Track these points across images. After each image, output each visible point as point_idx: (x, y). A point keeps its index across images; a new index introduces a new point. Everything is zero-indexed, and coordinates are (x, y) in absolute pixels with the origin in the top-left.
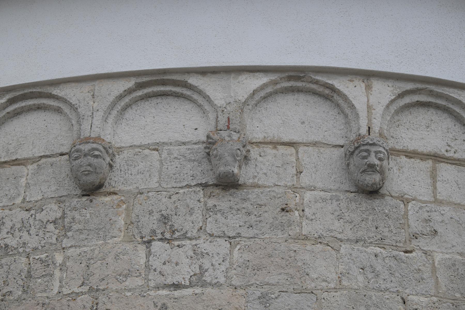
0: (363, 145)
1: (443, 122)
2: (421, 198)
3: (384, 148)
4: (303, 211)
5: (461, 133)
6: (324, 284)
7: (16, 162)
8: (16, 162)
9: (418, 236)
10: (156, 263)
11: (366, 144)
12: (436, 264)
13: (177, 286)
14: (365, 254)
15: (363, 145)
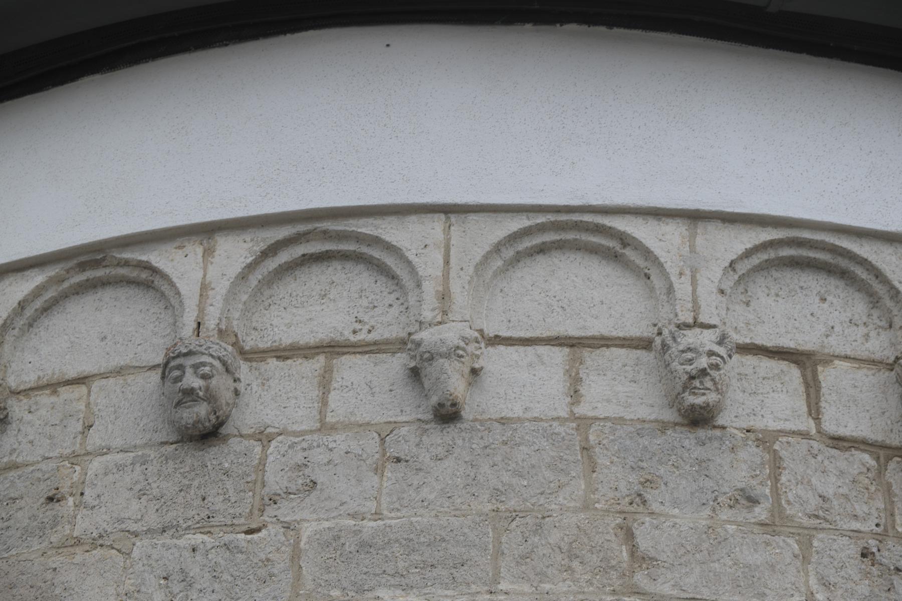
0: (174, 358)
1: (353, 281)
2: (296, 428)
3: (212, 356)
4: (82, 494)
5: (385, 294)
9: (277, 498)
11: (178, 356)
12: (302, 544)
14: (175, 550)
15: (174, 358)
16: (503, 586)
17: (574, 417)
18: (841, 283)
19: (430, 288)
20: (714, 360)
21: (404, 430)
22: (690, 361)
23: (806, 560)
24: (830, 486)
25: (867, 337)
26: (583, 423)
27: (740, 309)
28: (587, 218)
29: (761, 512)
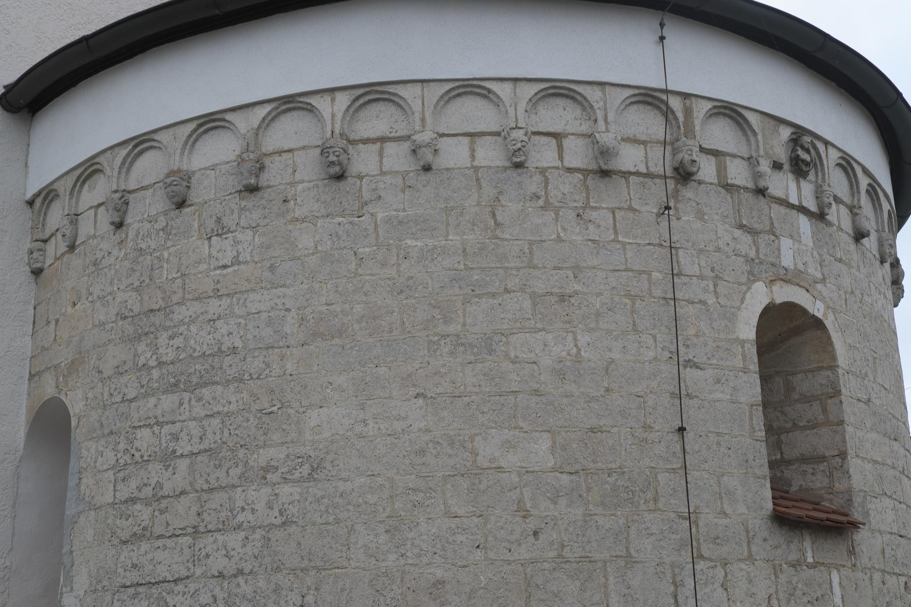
6: (306, 251)
7: (143, 188)
8: (143, 188)
10: (214, 252)
13: (225, 267)
16: (450, 237)
17: (473, 167)
18: (572, 102)
19: (417, 116)
20: (523, 144)
21: (411, 174)
22: (515, 145)
23: (557, 220)
24: (566, 189)
25: (581, 124)
26: (476, 169)
27: (533, 116)
28: (475, 83)
29: (541, 202)
